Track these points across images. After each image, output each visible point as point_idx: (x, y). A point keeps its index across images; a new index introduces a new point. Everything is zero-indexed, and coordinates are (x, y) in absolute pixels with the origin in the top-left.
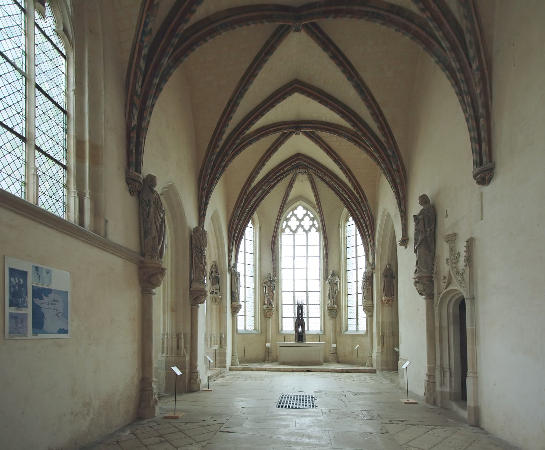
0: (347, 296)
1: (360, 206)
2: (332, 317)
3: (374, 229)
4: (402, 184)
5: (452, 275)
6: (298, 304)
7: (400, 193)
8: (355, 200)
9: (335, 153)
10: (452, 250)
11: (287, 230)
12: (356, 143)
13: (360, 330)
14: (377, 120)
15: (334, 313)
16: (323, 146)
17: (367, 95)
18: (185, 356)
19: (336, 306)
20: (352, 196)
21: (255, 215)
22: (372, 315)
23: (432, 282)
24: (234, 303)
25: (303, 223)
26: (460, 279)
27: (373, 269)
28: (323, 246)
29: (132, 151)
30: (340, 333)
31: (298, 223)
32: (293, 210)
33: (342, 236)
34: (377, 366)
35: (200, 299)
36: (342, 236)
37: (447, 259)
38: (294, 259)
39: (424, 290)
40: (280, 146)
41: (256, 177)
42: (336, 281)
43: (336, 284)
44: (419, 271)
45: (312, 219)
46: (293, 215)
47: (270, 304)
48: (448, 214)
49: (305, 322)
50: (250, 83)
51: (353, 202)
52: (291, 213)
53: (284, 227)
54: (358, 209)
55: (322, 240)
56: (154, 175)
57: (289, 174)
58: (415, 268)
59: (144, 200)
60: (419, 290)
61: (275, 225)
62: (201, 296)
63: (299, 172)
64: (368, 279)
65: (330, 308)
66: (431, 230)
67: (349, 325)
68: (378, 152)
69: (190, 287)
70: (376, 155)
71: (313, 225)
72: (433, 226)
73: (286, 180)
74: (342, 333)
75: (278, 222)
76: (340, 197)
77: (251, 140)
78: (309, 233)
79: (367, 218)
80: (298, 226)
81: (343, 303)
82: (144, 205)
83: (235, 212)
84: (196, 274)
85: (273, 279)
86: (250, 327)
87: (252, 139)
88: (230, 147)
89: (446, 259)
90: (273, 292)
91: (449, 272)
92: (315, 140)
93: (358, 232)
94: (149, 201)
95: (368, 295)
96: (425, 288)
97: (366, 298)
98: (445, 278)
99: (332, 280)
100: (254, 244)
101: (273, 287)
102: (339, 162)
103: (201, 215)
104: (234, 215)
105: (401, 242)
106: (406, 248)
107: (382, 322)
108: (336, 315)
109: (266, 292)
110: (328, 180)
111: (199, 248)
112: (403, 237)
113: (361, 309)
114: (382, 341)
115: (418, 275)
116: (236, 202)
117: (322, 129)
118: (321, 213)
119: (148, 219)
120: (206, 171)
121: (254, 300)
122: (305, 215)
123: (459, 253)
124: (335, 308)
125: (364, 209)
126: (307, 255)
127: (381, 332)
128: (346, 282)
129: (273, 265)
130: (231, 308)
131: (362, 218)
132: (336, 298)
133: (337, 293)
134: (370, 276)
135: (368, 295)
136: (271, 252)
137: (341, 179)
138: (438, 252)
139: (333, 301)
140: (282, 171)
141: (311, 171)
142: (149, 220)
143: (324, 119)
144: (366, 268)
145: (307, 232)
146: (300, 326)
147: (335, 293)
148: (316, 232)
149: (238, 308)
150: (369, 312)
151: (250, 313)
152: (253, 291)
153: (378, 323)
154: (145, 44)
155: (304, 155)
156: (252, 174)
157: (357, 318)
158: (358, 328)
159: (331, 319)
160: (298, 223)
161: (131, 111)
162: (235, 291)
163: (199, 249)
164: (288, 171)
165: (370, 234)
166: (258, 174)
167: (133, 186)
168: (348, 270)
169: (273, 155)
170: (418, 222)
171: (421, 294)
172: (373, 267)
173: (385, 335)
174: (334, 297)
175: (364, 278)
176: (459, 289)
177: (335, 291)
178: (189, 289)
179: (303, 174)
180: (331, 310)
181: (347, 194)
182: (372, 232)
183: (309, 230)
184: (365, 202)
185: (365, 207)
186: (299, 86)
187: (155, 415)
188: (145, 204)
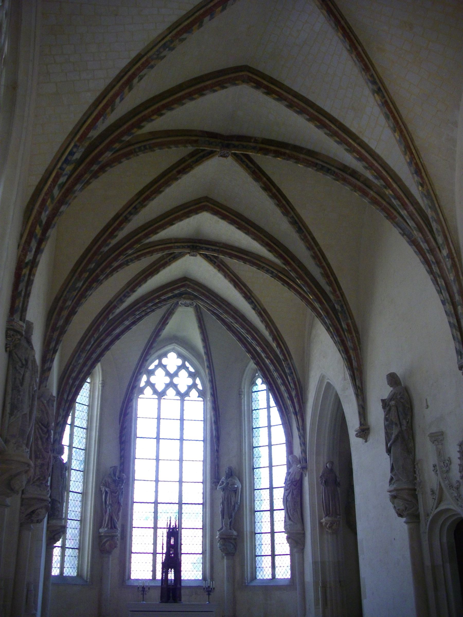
0: (254, 514)
1: (281, 365)
3: (303, 403)
4: (355, 349)
5: (445, 489)
7: (353, 361)
8: (273, 356)
9: (245, 286)
10: (440, 454)
11: (148, 391)
12: (285, 283)
13: (279, 578)
14: (320, 265)
15: (232, 546)
16: (229, 275)
17: (307, 234)
19: (235, 533)
20: (268, 349)
23: (415, 497)
24: (54, 522)
25: (176, 380)
26: (456, 495)
27: (304, 468)
28: (211, 423)
29: (20, 293)
31: (167, 380)
32: (160, 358)
33: (246, 409)
36: (245, 408)
37: (433, 465)
39: (406, 509)
41: (118, 308)
42: (236, 486)
43: (235, 491)
44: (397, 481)
45: (191, 375)
46: (160, 365)
48: (429, 404)
50: (151, 199)
51: (268, 357)
52: (156, 362)
53: (142, 384)
54: (277, 370)
57: (165, 305)
58: (389, 475)
60: (399, 510)
64: (294, 486)
65: (224, 537)
66: (408, 422)
67: (258, 568)
68: (321, 303)
70: (317, 305)
71: (194, 385)
72: (409, 417)
73: (159, 313)
74: (245, 583)
76: (246, 346)
77: (127, 260)
78: (187, 398)
79: (292, 385)
80: (168, 386)
82: (17, 366)
85: (119, 478)
86: (71, 571)
89: (432, 466)
91: (440, 485)
92: (217, 266)
93: (272, 403)
94: (27, 361)
96: (407, 506)
97: (292, 519)
98: (433, 492)
99: (228, 484)
100: (89, 410)
101: (120, 493)
102: (251, 299)
103: (45, 368)
104: (73, 363)
105: (360, 433)
106: (366, 441)
107: (323, 563)
108: (236, 549)
109: (106, 502)
110: (229, 320)
112: (361, 424)
115: (395, 486)
116: (79, 343)
117: (231, 256)
118: (211, 367)
120: (65, 301)
121: (81, 517)
123: (449, 458)
124: (234, 537)
125: (287, 371)
127: (322, 580)
131: (284, 384)
133: (236, 508)
136: (118, 426)
137: (250, 322)
138: (419, 455)
139: (230, 523)
141: (200, 304)
143: (237, 244)
145: (183, 396)
147: (234, 508)
148: (199, 397)
149: (59, 533)
152: (80, 499)
154: (65, 172)
155: (194, 280)
159: (225, 557)
160: (167, 380)
161: (28, 242)
163: (46, 427)
164: (165, 300)
165: (297, 411)
167: (12, 339)
169: (150, 279)
170: (390, 410)
171: (400, 515)
172: (304, 464)
173: (328, 586)
174: (231, 516)
175: (288, 483)
176: (454, 509)
177: (233, 504)
179: (188, 306)
181: (259, 344)
182: (300, 407)
183: (187, 393)
184: (289, 360)
185: (290, 368)
186: (210, 205)
188: (20, 364)
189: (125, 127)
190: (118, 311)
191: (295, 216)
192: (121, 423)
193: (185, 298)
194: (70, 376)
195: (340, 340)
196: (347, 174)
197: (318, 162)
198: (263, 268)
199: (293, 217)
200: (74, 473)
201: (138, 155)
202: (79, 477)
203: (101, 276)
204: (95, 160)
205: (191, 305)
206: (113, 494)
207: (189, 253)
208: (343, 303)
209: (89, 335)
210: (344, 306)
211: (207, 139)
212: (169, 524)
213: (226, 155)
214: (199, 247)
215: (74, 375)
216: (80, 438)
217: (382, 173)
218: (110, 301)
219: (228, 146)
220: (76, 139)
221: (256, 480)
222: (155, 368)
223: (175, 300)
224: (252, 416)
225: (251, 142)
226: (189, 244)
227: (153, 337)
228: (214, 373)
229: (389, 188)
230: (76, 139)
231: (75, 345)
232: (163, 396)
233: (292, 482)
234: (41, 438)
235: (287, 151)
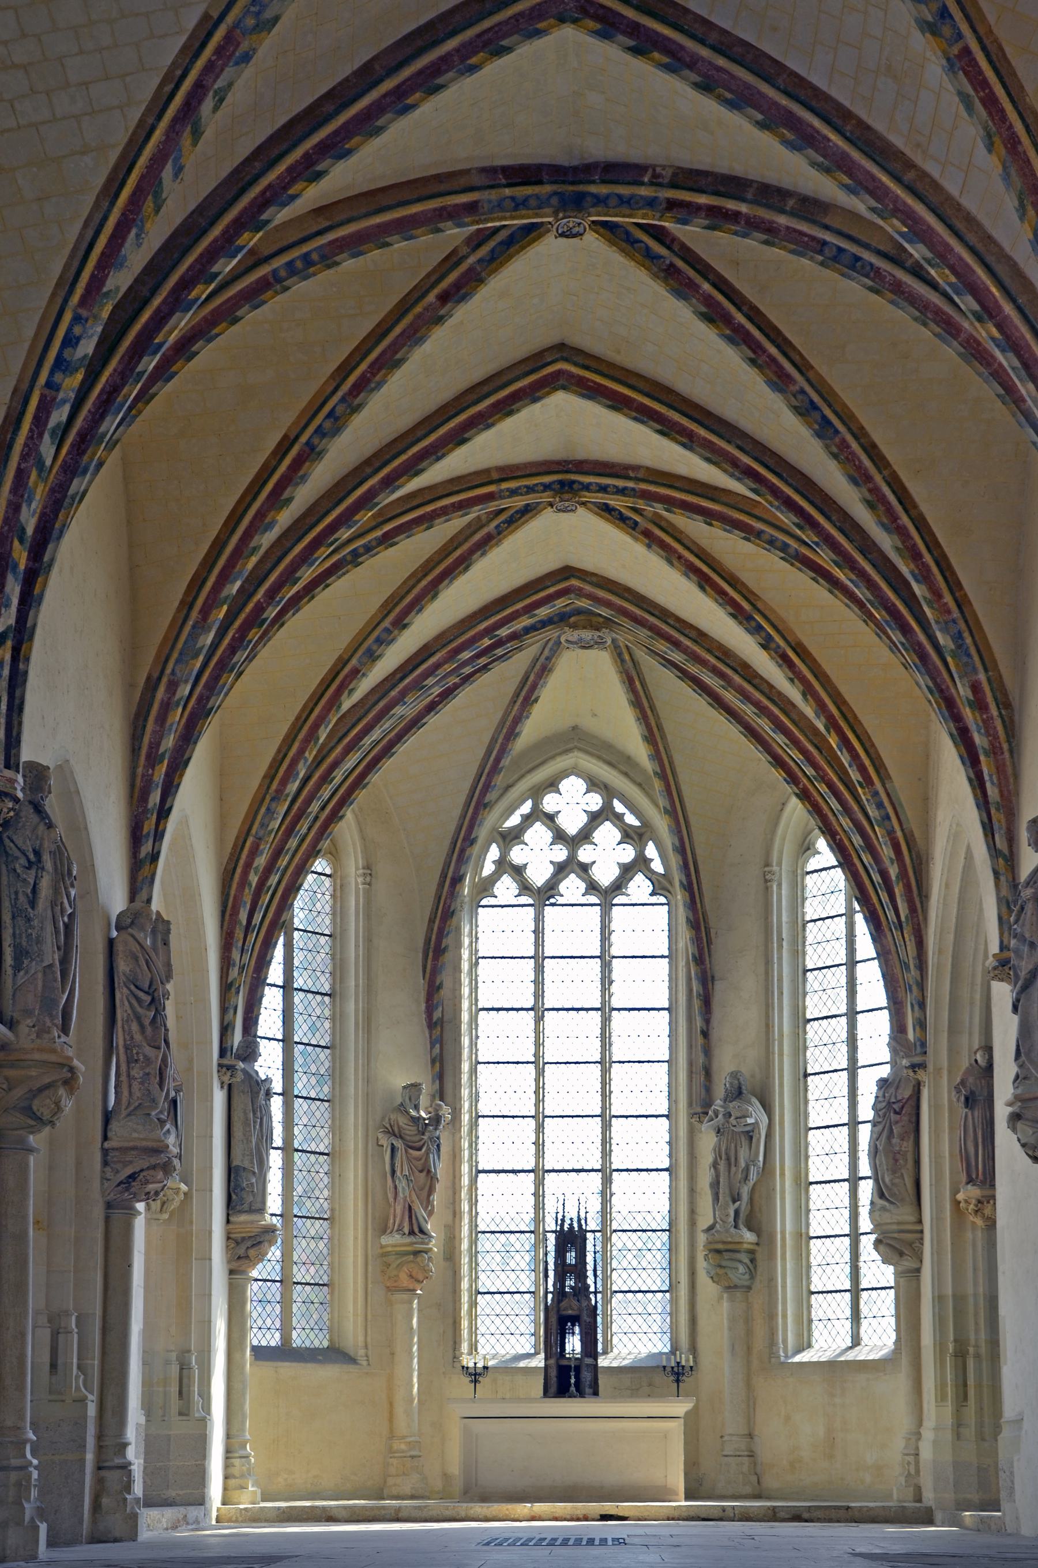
2: (731, 1288)
6: (558, 1228)
9: (733, 581)
11: (506, 888)
18: (82, 1401)
19: (749, 1237)
21: (347, 827)
22: (918, 1270)
28: (688, 963)
30: (770, 1358)
32: (537, 793)
34: (935, 1490)
35: (147, 1182)
38: (539, 1019)
40: (483, 554)
41: (364, 675)
42: (750, 1121)
43: (750, 1136)
45: (628, 835)
46: (537, 815)
47: (417, 1230)
49: (595, 1307)
50: (373, 385)
55: (685, 935)
56: (45, 764)
57: (519, 649)
59: (19, 849)
61: (447, 865)
62: (151, 1172)
63: (570, 639)
64: (896, 1112)
69: (105, 1138)
71: (640, 863)
74: (779, 1357)
75: (462, 851)
80: (561, 870)
81: (784, 1223)
82: (17, 866)
83: (259, 817)
84: (130, 1086)
86: (312, 1336)
87: (364, 546)
88: (272, 594)
90: (429, 1171)
94: (37, 853)
95: (897, 1181)
100: (333, 948)
104: (253, 831)
107: (959, 1299)
108: (752, 1277)
109: (393, 1172)
111: (146, 987)
113: (867, 1243)
114: (956, 1376)
115: (1019, 1091)
119: (33, 908)
120: (173, 686)
122: (595, 819)
124: (745, 1246)
125: (872, 812)
126: (603, 1002)
128: (802, 1128)
129: (432, 1047)
130: (228, 1238)
132: (751, 1200)
133: (753, 1176)
134: (908, 1099)
135: (897, 1181)
136: (422, 984)
139: (737, 1213)
140: (487, 642)
142: (36, 912)
144: (893, 1063)
146: (573, 1325)
147: (746, 1178)
150: (901, 1254)
151: (312, 1270)
153: (939, 1299)
154: (61, 395)
156: (348, 660)
157: (856, 1291)
158: (858, 1333)
162: (246, 1164)
165: (903, 919)
166: (374, 661)
168: (809, 1071)
169: (447, 586)
172: (917, 1060)
173: (971, 1350)
175: (880, 1106)
177: (743, 1164)
178: (100, 1145)
179: (590, 647)
180: (727, 1255)
182: (912, 909)
183: (619, 886)
185: (880, 805)
186: (574, 370)
187: (37, 1553)
188: (23, 861)
189: (216, 231)
190: (364, 686)
191: (808, 389)
192: (427, 976)
193: (574, 627)
194: (248, 865)
195: (958, 729)
196: (904, 268)
197: (828, 237)
198: (759, 534)
199: (802, 391)
200: (305, 1106)
201: (286, 289)
202: (318, 1114)
203: (270, 608)
204: (143, 346)
205: (600, 644)
206: (411, 1151)
207: (551, 505)
208: (962, 625)
209: (291, 754)
210: (966, 634)
211: (507, 192)
212: (560, 1217)
213: (576, 229)
214: (580, 483)
215: (261, 861)
216: (314, 1019)
217: (974, 271)
218: (340, 658)
219: (577, 203)
220: (75, 299)
221: (811, 1104)
222: (521, 822)
223: (551, 633)
224: (804, 938)
225: (642, 184)
226: (547, 479)
227: (500, 741)
228: (688, 826)
229: (991, 317)
230: (75, 299)
231: (255, 783)
232: (548, 899)
233: (889, 1103)
234: (138, 1019)
235: (743, 208)
